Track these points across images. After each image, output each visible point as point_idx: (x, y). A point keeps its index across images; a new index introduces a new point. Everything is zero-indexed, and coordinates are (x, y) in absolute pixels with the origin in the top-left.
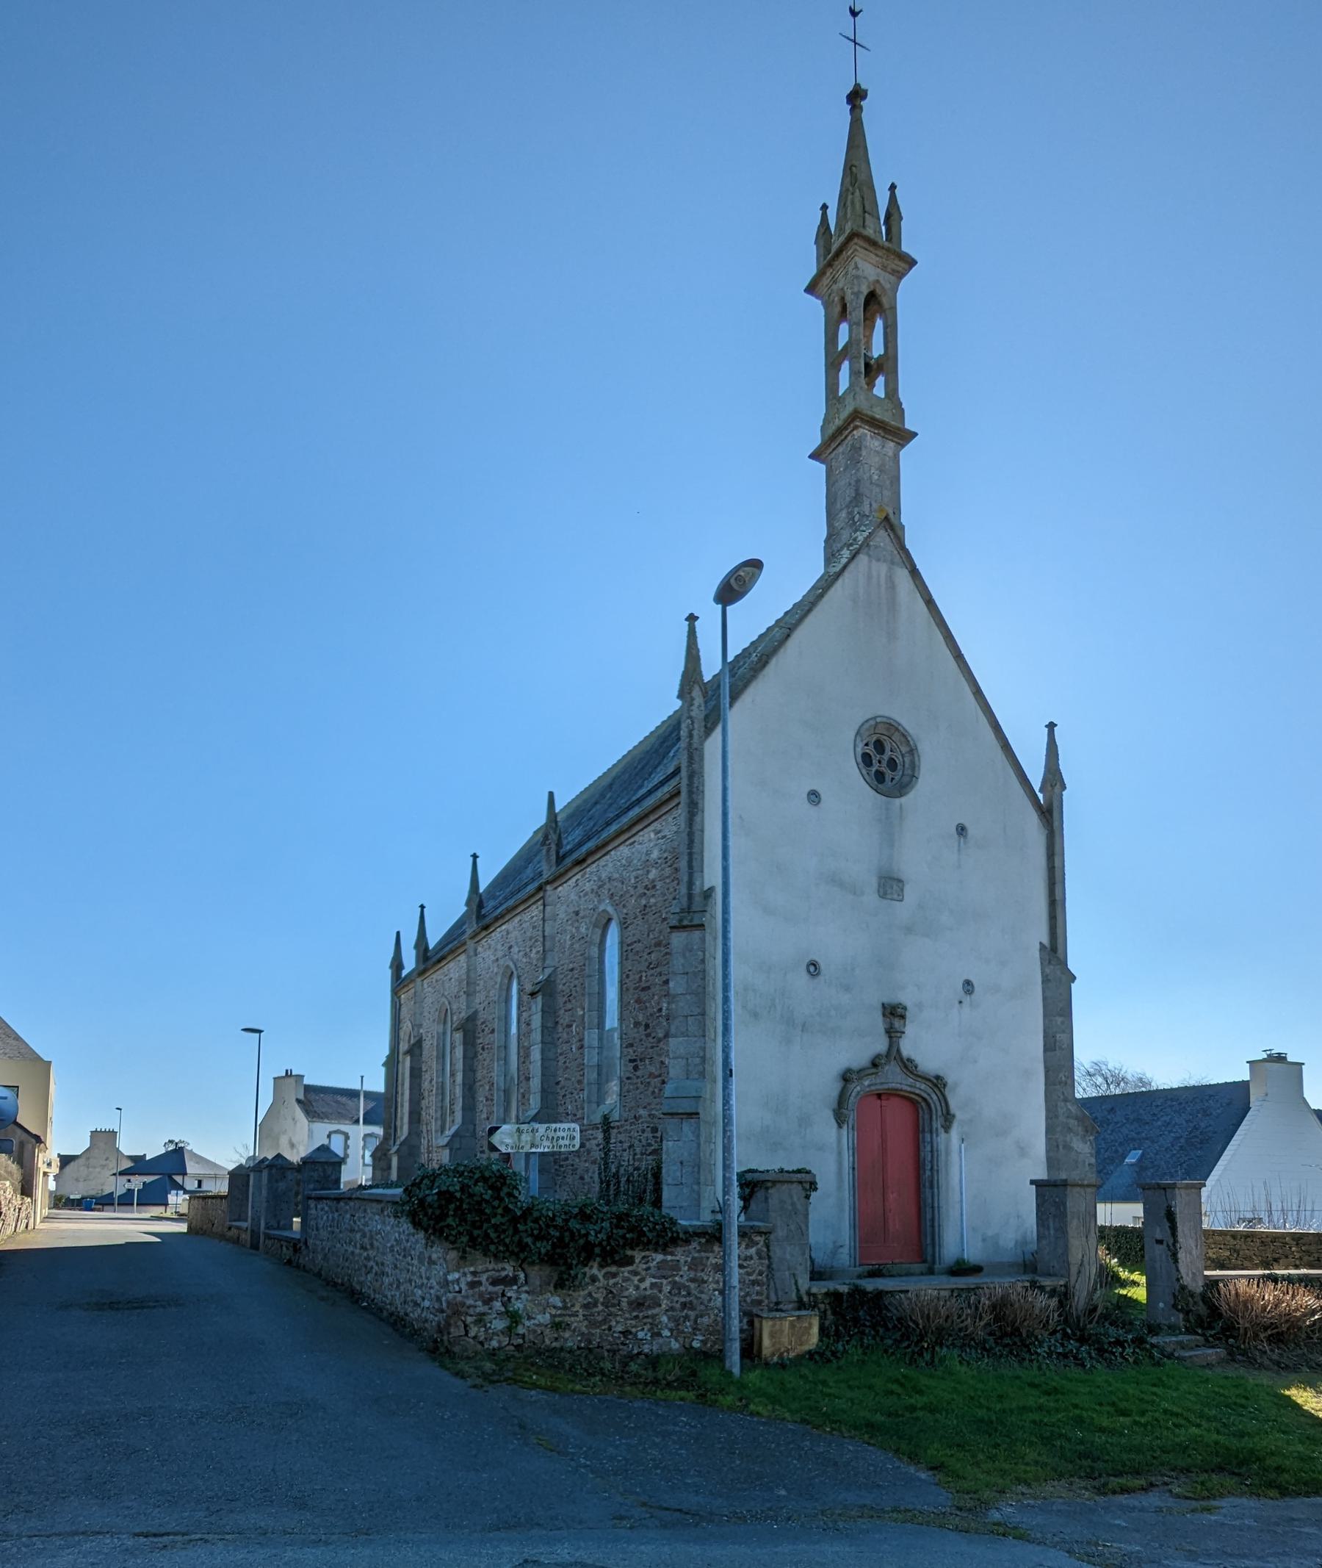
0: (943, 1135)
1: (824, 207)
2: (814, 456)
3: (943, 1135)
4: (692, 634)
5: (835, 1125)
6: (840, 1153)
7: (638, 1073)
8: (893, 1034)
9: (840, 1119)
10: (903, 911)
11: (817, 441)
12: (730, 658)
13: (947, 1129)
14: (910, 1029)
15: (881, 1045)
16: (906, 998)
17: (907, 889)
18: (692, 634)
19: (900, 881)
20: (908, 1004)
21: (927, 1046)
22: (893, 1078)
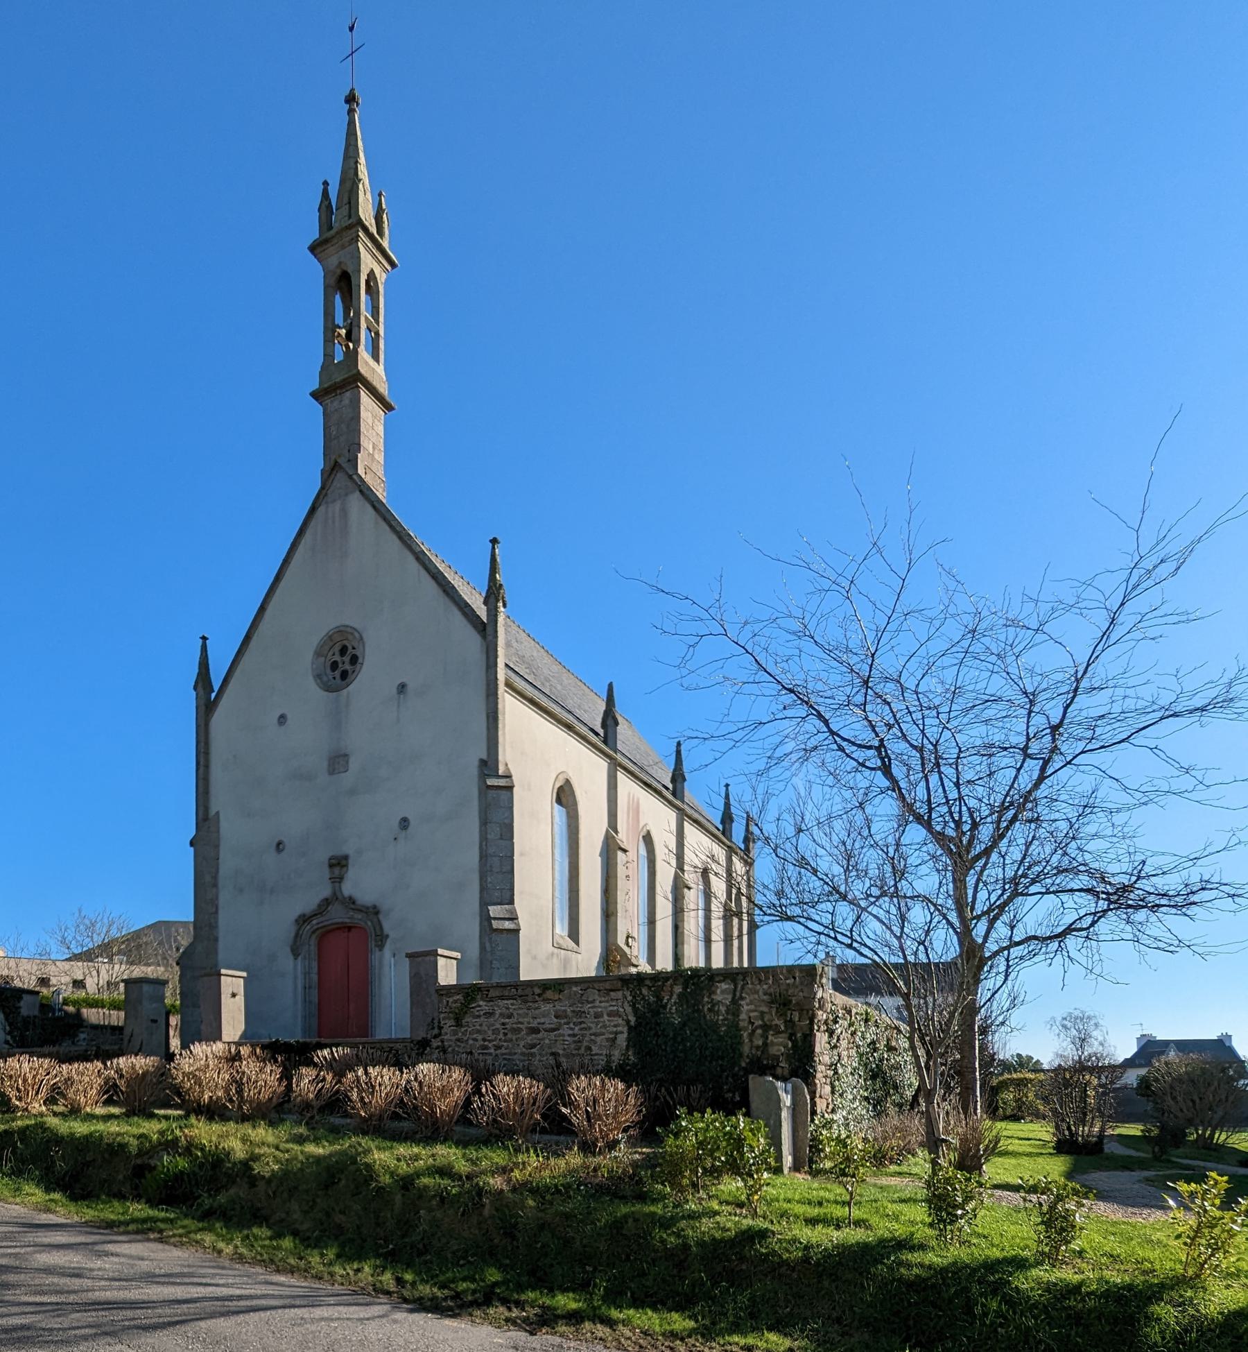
0: (378, 953)
1: (326, 183)
2: (314, 395)
3: (378, 953)
4: (204, 649)
5: (292, 957)
6: (295, 978)
7: (1143, 858)
8: (337, 880)
9: (295, 952)
10: (347, 779)
11: (315, 385)
12: (365, 399)
13: (381, 947)
14: (352, 873)
15: (326, 892)
16: (348, 849)
17: (351, 760)
18: (204, 649)
19: (346, 755)
20: (351, 852)
21: (362, 884)
22: (338, 914)
